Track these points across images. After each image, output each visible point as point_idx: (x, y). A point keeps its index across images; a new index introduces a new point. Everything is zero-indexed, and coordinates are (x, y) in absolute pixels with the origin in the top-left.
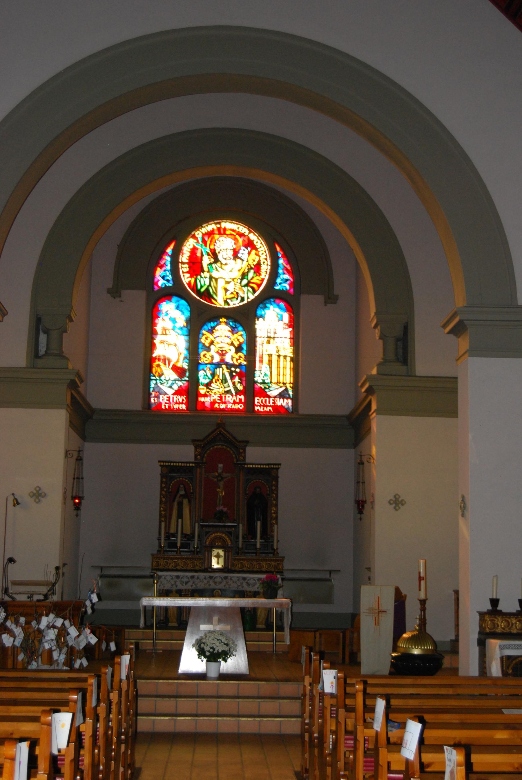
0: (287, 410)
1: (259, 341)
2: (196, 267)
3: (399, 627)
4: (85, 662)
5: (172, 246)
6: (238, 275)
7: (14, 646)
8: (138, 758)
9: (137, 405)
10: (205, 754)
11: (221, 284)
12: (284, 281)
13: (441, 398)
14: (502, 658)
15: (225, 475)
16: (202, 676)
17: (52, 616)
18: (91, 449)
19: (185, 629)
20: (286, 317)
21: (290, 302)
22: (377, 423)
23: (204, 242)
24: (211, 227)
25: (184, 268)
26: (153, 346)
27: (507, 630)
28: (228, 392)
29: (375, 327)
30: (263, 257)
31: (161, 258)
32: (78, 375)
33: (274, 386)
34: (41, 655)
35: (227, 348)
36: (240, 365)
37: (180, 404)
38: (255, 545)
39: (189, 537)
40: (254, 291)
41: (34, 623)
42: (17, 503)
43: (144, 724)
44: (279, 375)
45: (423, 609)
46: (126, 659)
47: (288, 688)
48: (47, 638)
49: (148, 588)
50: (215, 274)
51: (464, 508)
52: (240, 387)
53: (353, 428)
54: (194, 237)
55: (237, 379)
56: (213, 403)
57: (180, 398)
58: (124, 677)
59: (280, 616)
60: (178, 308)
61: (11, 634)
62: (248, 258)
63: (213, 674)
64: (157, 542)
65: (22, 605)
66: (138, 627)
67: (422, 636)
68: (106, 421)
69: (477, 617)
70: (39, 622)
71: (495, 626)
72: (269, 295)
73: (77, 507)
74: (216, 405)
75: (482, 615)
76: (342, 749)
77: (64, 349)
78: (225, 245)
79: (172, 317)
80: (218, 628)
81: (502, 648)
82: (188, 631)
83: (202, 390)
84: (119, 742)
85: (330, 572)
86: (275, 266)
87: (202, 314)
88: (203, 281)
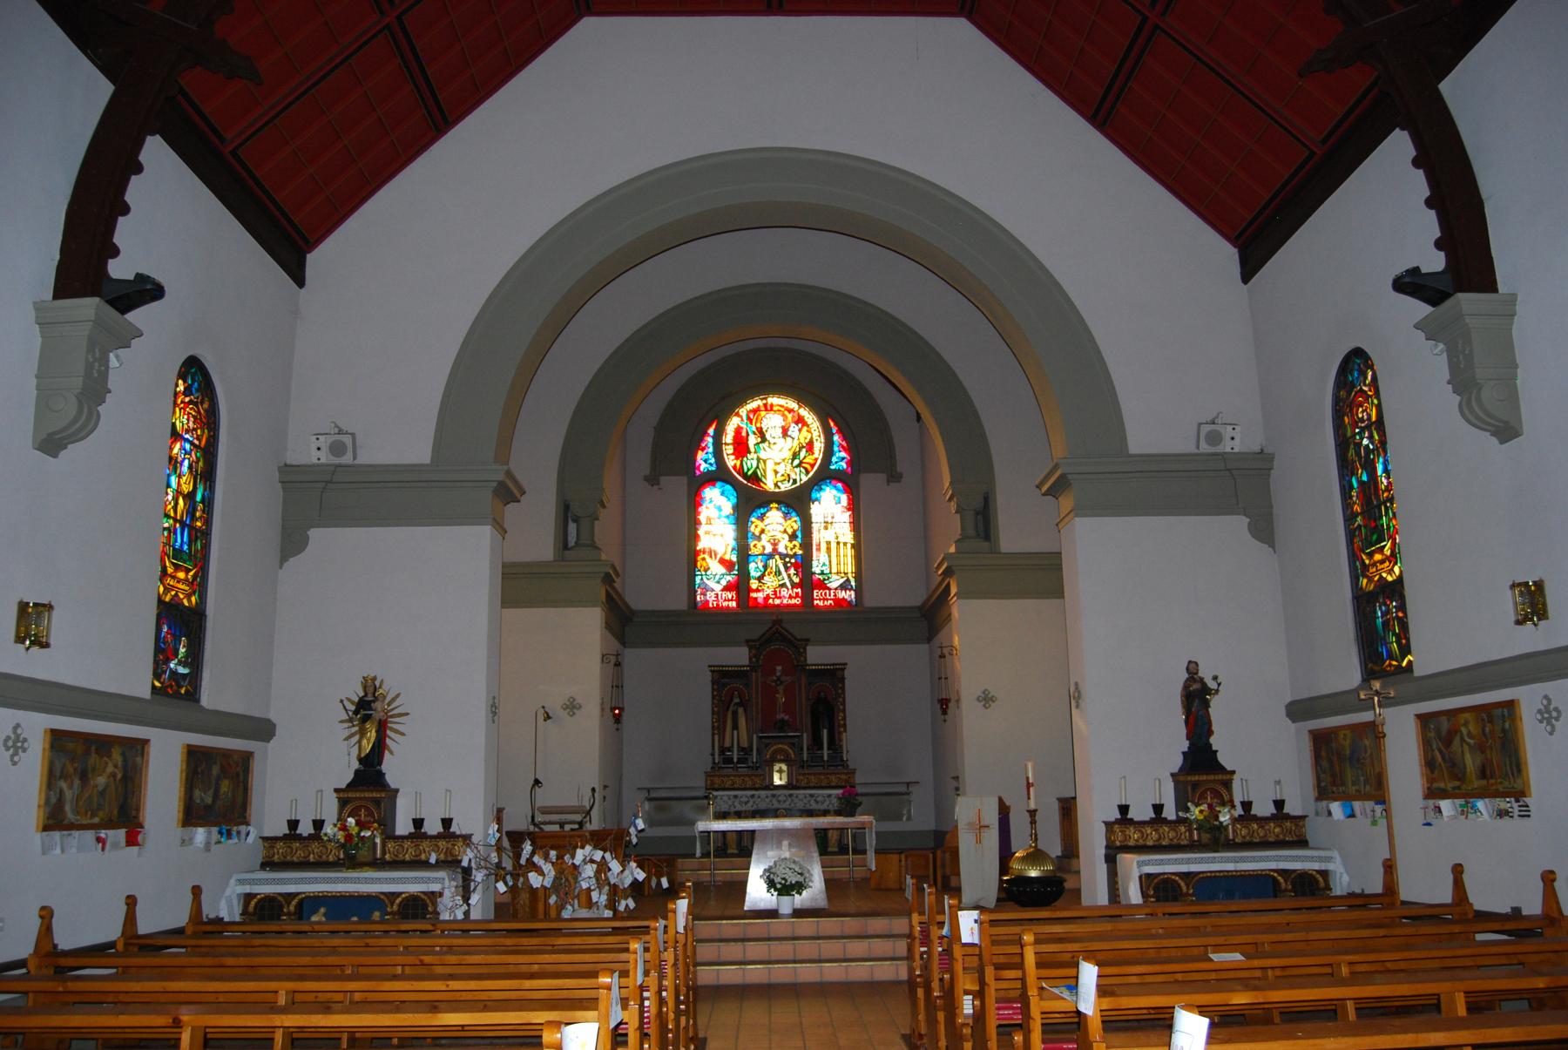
0: (849, 603)
1: (815, 527)
2: (741, 448)
4: (632, 904)
6: (789, 455)
9: (681, 604)
10: (784, 1013)
11: (770, 467)
12: (840, 461)
16: (772, 914)
17: (588, 848)
18: (631, 656)
19: (750, 855)
20: (844, 498)
21: (848, 482)
22: (959, 609)
23: (750, 420)
24: (756, 403)
25: (728, 450)
26: (697, 537)
27: (1141, 842)
28: (783, 585)
29: (951, 499)
30: (815, 434)
31: (702, 440)
33: (834, 577)
34: (578, 896)
35: (779, 536)
37: (730, 601)
39: (746, 751)
40: (807, 472)
41: (567, 857)
43: (706, 975)
44: (839, 564)
45: (1033, 822)
46: (682, 905)
49: (703, 810)
50: (762, 455)
52: (796, 580)
53: (928, 620)
54: (738, 414)
55: (792, 571)
56: (768, 597)
58: (681, 930)
61: (540, 872)
62: (799, 436)
65: (553, 835)
66: (693, 855)
68: (648, 623)
70: (573, 857)
72: (824, 475)
73: (618, 719)
75: (1108, 825)
78: (772, 423)
79: (717, 504)
80: (787, 855)
81: (1140, 864)
83: (754, 584)
84: (678, 1013)
87: (751, 498)
88: (750, 463)
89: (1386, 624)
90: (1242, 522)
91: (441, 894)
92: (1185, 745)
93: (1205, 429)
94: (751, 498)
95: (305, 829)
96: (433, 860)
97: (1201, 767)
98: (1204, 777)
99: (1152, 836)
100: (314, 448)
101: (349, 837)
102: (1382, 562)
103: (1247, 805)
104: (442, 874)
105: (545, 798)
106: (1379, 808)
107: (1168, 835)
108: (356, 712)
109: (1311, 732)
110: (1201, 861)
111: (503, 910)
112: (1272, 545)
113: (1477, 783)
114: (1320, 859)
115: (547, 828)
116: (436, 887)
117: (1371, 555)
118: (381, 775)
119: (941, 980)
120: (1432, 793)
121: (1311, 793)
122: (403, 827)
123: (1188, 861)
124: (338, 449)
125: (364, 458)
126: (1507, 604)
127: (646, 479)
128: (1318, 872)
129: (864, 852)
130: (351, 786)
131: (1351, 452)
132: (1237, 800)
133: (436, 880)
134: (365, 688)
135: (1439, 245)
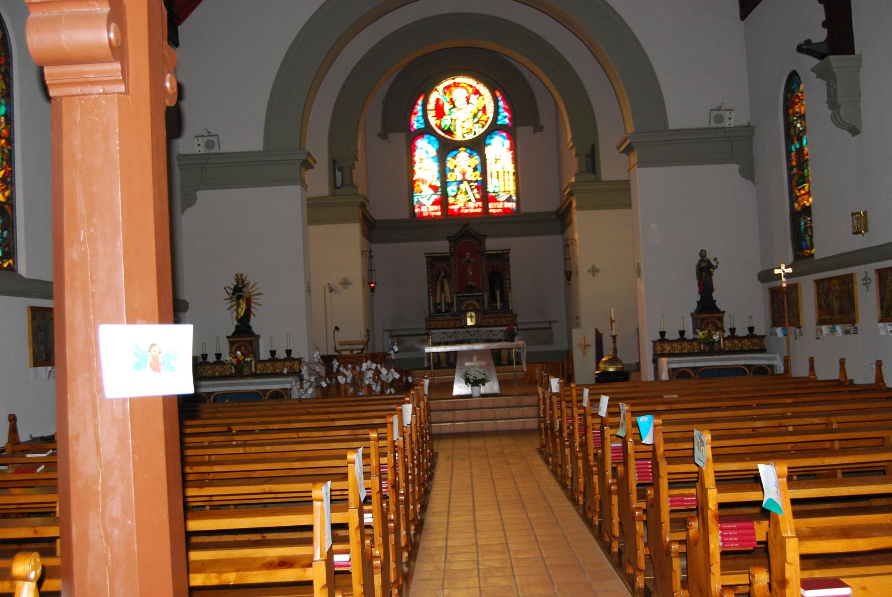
3: (599, 354)
4: (393, 391)
5: (422, 98)
7: (346, 383)
8: (435, 447)
9: (405, 215)
11: (458, 124)
12: (504, 119)
13: (619, 195)
14: (669, 370)
15: (472, 260)
17: (369, 362)
18: (377, 248)
20: (507, 143)
21: (510, 131)
22: (577, 216)
24: (450, 82)
25: (431, 114)
26: (413, 172)
28: (470, 201)
29: (572, 148)
31: (414, 108)
32: (365, 198)
36: (476, 181)
38: (496, 307)
41: (357, 368)
42: (331, 290)
43: (436, 428)
45: (615, 342)
47: (527, 400)
48: (367, 377)
49: (425, 343)
50: (454, 116)
51: (639, 272)
53: (559, 221)
55: (475, 191)
56: (460, 209)
57: (437, 208)
59: (518, 355)
60: (429, 143)
61: (345, 376)
63: (476, 394)
64: (427, 310)
65: (346, 357)
67: (613, 361)
69: (651, 344)
70: (361, 367)
71: (663, 349)
72: (494, 128)
74: (462, 211)
75: (654, 342)
76: (565, 426)
77: (354, 180)
79: (425, 151)
82: (457, 370)
83: (451, 200)
85: (550, 322)
86: (497, 107)
87: (447, 147)
88: (446, 122)
89: (806, 229)
90: (736, 167)
91: (291, 389)
92: (698, 297)
93: (714, 113)
94: (447, 147)
95: (212, 359)
96: (285, 371)
97: (707, 310)
98: (707, 316)
99: (678, 348)
100: (196, 144)
101: (239, 361)
102: (804, 195)
103: (732, 330)
104: (290, 379)
105: (341, 337)
106: (798, 331)
107: (687, 347)
108: (233, 294)
109: (770, 289)
110: (702, 361)
111: (325, 393)
112: (753, 181)
113: (838, 317)
114: (769, 359)
115: (344, 353)
116: (288, 386)
117: (799, 190)
118: (250, 327)
119: (596, 455)
120: (821, 322)
121: (770, 323)
122: (264, 355)
123: (695, 361)
124: (210, 145)
125: (225, 149)
126: (848, 224)
127: (379, 135)
128: (768, 365)
129: (521, 364)
130: (234, 335)
131: (792, 131)
132: (727, 327)
133: (287, 382)
134: (237, 281)
135: (824, 25)
